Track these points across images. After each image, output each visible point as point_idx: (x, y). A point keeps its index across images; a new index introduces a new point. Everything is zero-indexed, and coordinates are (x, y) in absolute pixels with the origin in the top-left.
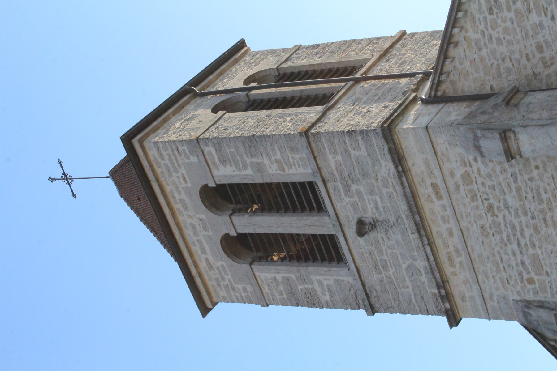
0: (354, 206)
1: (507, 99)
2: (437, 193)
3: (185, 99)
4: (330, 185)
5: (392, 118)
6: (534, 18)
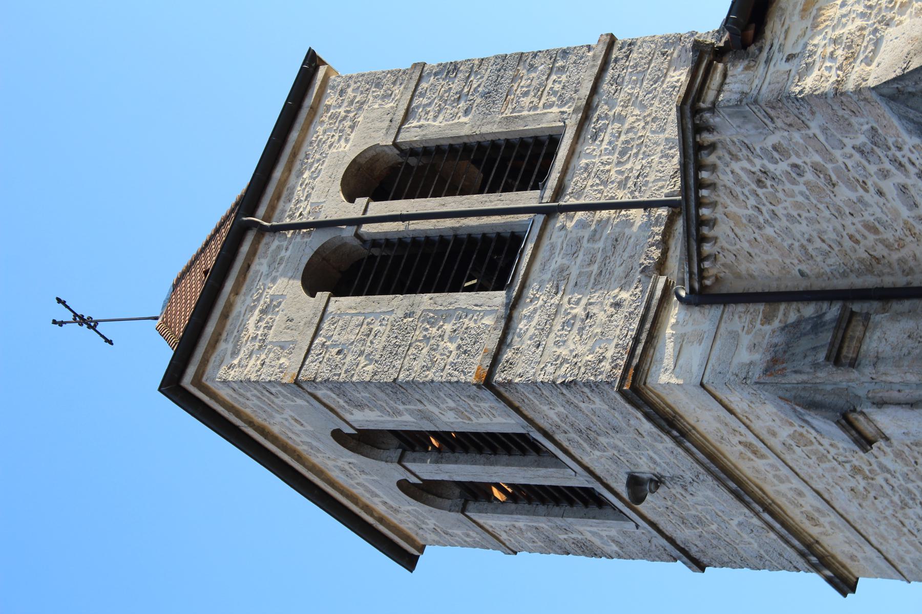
0: (615, 460)
1: (834, 353)
2: (755, 453)
3: (245, 248)
4: (559, 437)
5: (635, 361)
6: (844, 193)
